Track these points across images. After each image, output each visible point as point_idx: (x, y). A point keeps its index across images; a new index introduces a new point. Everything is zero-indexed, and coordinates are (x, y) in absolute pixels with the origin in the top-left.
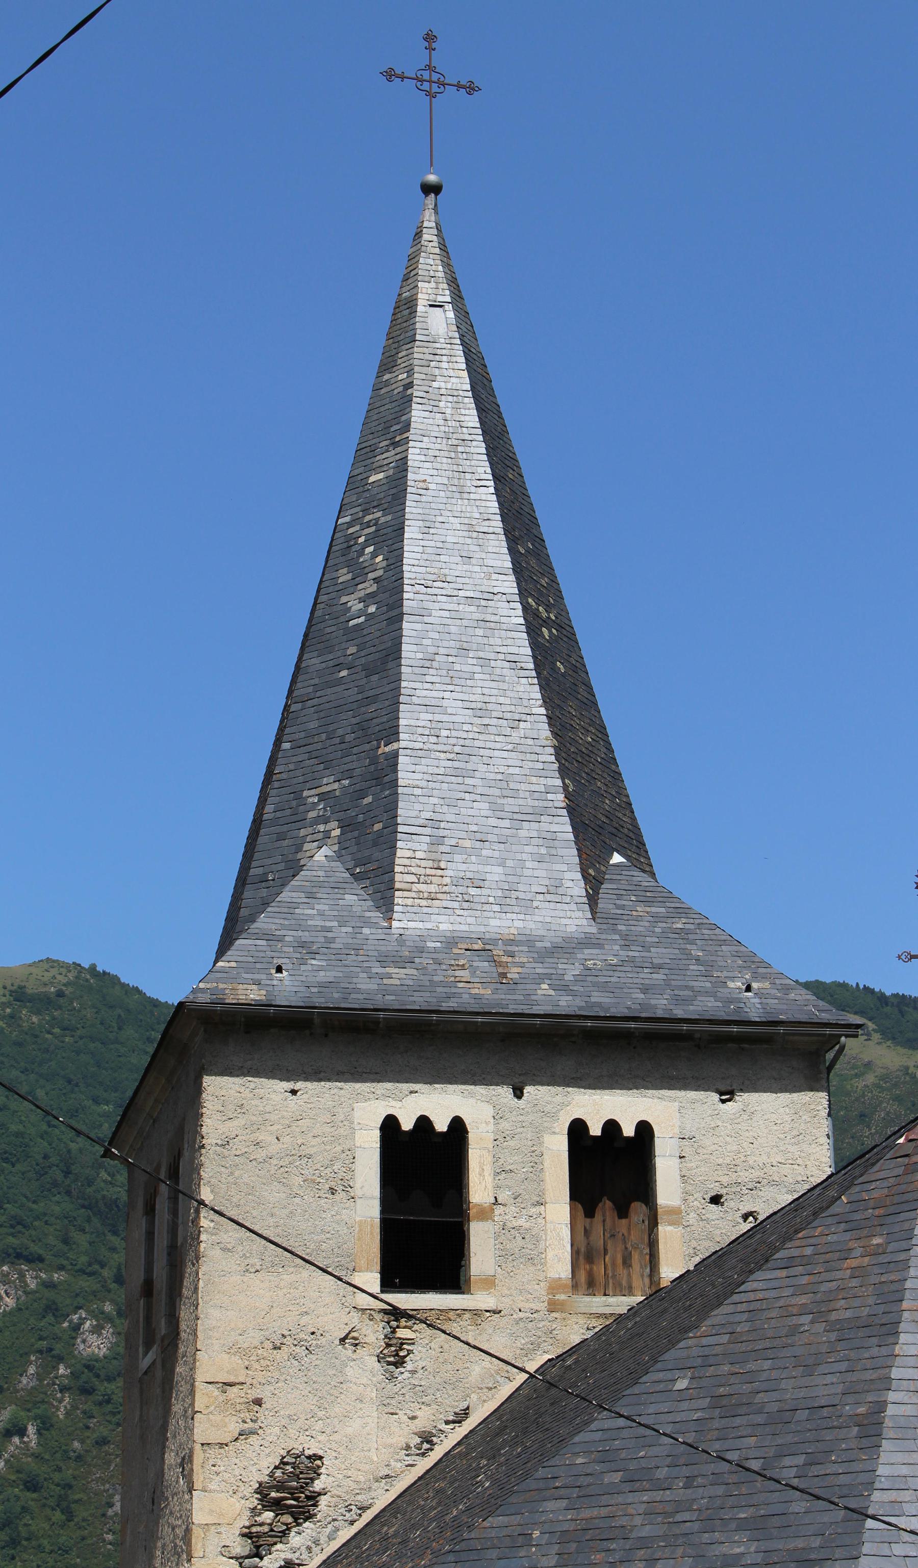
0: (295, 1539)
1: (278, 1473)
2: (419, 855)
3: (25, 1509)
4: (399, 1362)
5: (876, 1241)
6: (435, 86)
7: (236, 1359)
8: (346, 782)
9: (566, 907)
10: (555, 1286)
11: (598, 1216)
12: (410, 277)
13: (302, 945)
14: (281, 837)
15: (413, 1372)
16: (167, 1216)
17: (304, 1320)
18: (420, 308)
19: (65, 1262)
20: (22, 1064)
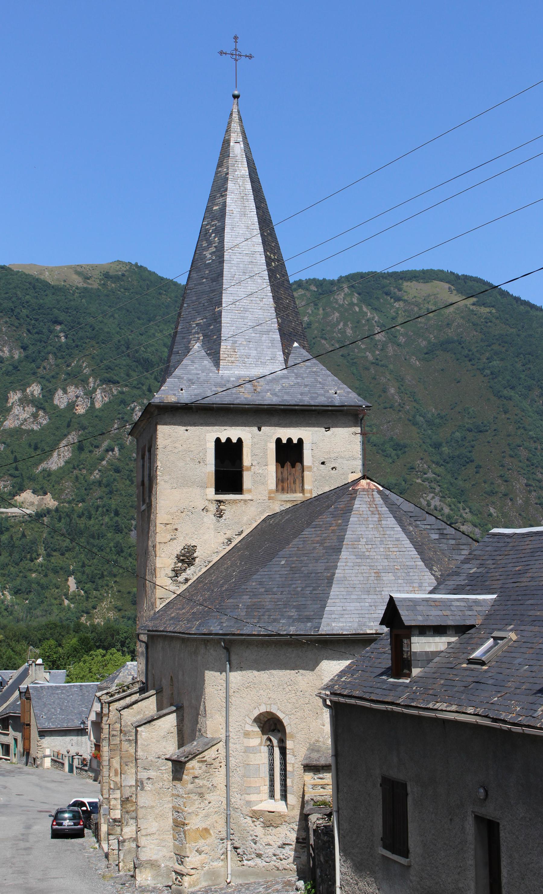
0: (188, 571)
1: (183, 551)
2: (229, 347)
3: (115, 480)
4: (221, 517)
5: (340, 522)
6: (237, 56)
7: (169, 516)
8: (205, 320)
9: (277, 364)
10: (270, 492)
11: (285, 468)
12: (228, 131)
13: (190, 380)
14: (183, 338)
15: (225, 519)
16: (148, 465)
17: (191, 504)
18: (232, 144)
19: (128, 384)
20: (109, 304)
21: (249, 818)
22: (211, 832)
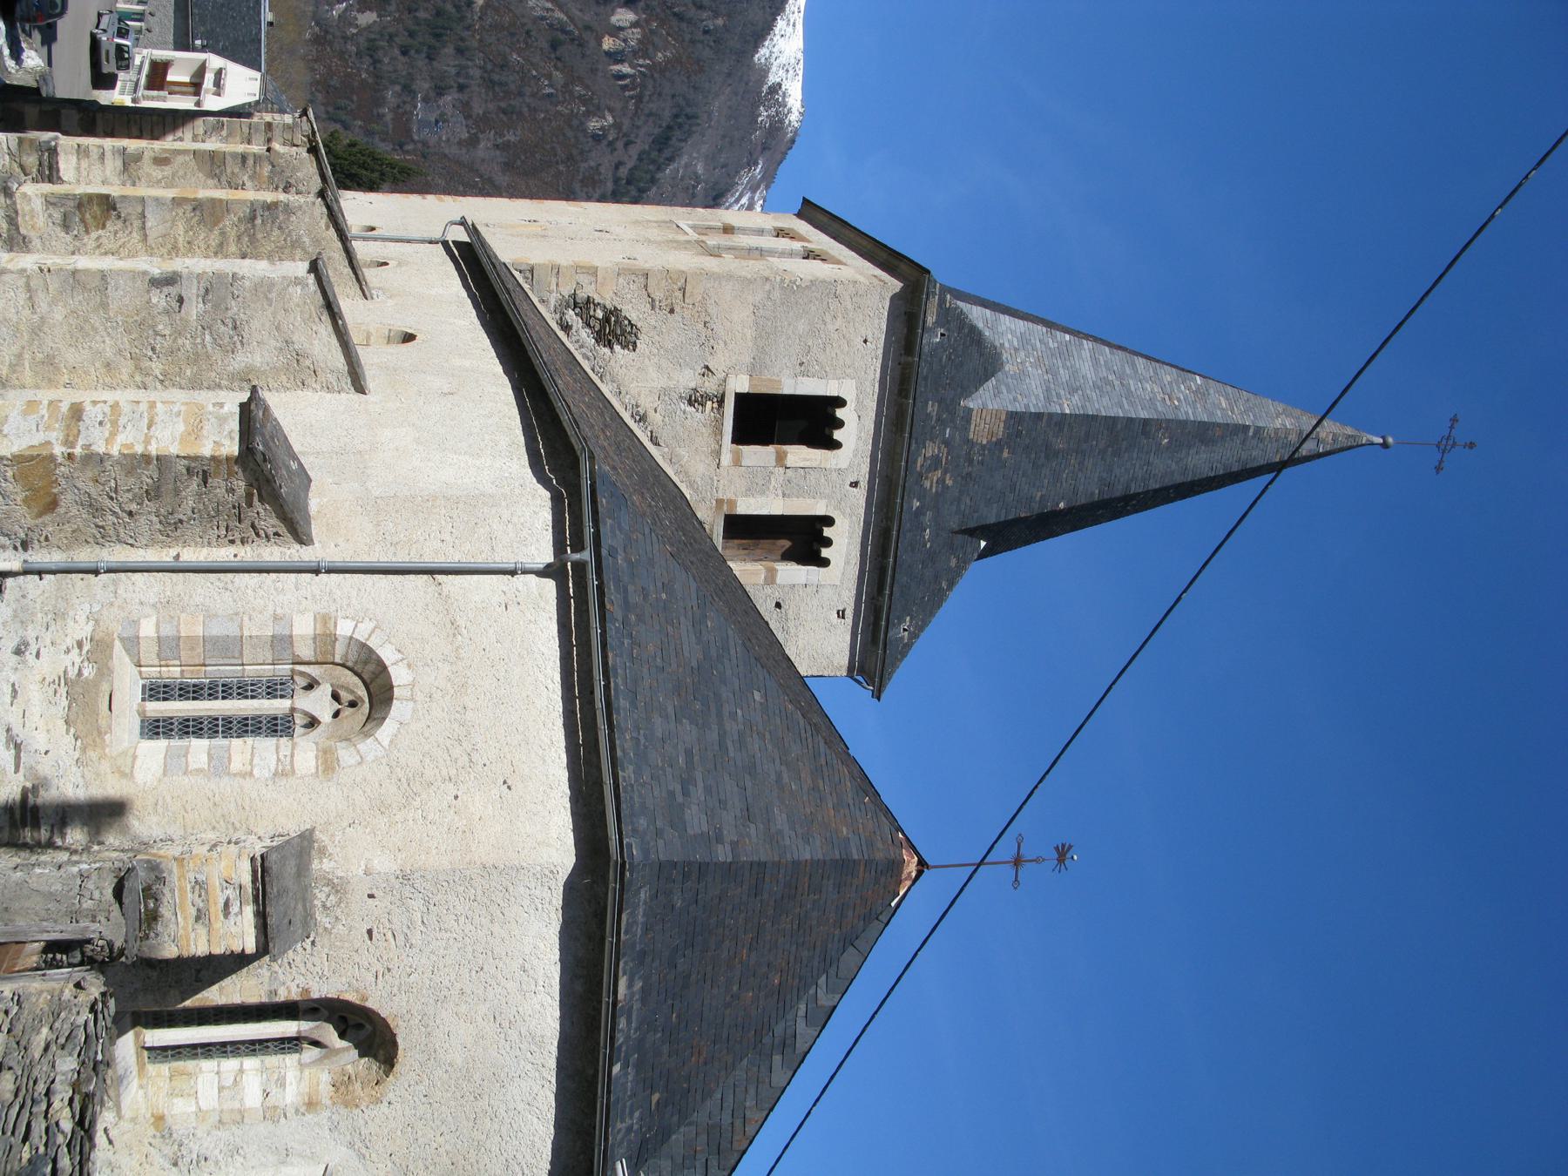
4: (690, 403)
10: (732, 503)
21: (89, 628)
22: (47, 518)
